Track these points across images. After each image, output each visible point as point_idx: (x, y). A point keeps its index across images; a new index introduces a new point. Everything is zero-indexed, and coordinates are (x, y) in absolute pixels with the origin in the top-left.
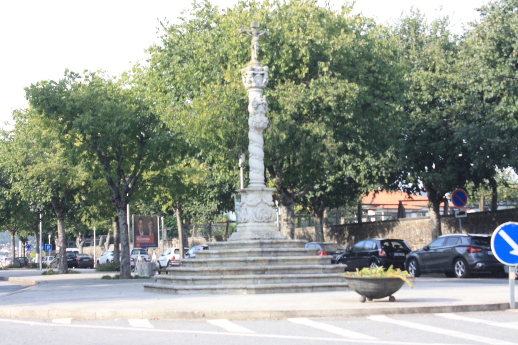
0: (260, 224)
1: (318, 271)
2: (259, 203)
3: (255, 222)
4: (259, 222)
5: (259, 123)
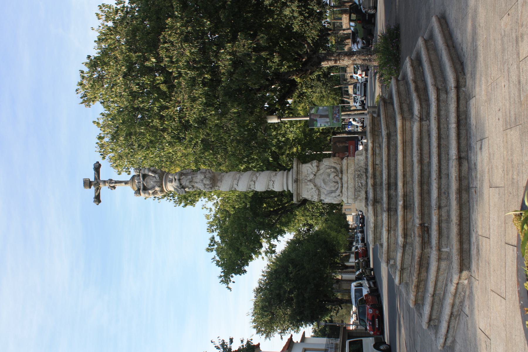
0: (345, 186)
1: (425, 128)
2: (315, 186)
3: (341, 192)
4: (342, 187)
5: (205, 185)
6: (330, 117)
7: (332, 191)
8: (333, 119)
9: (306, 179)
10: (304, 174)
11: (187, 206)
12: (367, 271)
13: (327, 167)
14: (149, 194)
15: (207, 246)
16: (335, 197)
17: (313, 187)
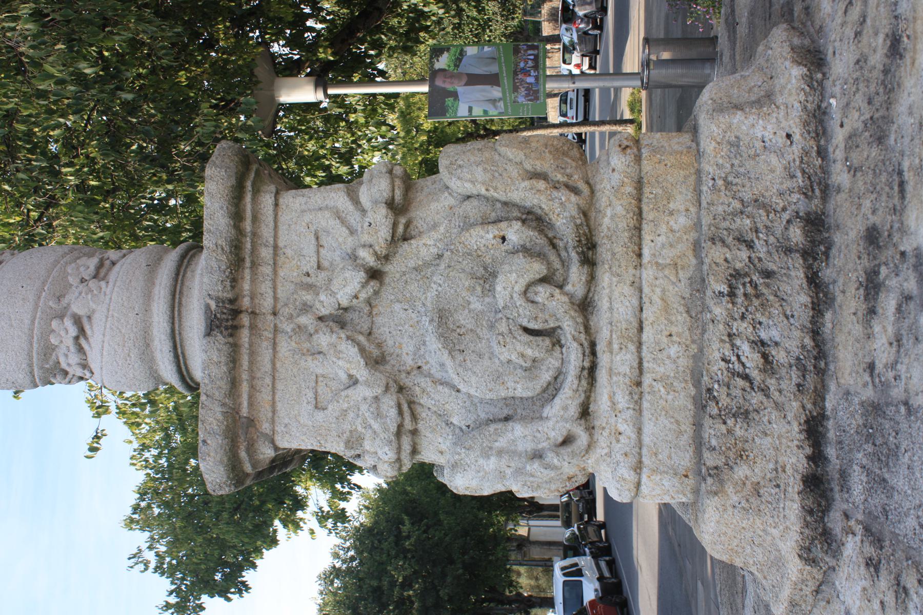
0: (616, 362)
2: (376, 360)
3: (585, 413)
4: (591, 372)
6: (506, 81)
7: (509, 401)
8: (515, 89)
9: (306, 308)
10: (289, 272)
12: (590, 529)
13: (472, 209)
15: (129, 511)
16: (537, 455)
17: (361, 372)
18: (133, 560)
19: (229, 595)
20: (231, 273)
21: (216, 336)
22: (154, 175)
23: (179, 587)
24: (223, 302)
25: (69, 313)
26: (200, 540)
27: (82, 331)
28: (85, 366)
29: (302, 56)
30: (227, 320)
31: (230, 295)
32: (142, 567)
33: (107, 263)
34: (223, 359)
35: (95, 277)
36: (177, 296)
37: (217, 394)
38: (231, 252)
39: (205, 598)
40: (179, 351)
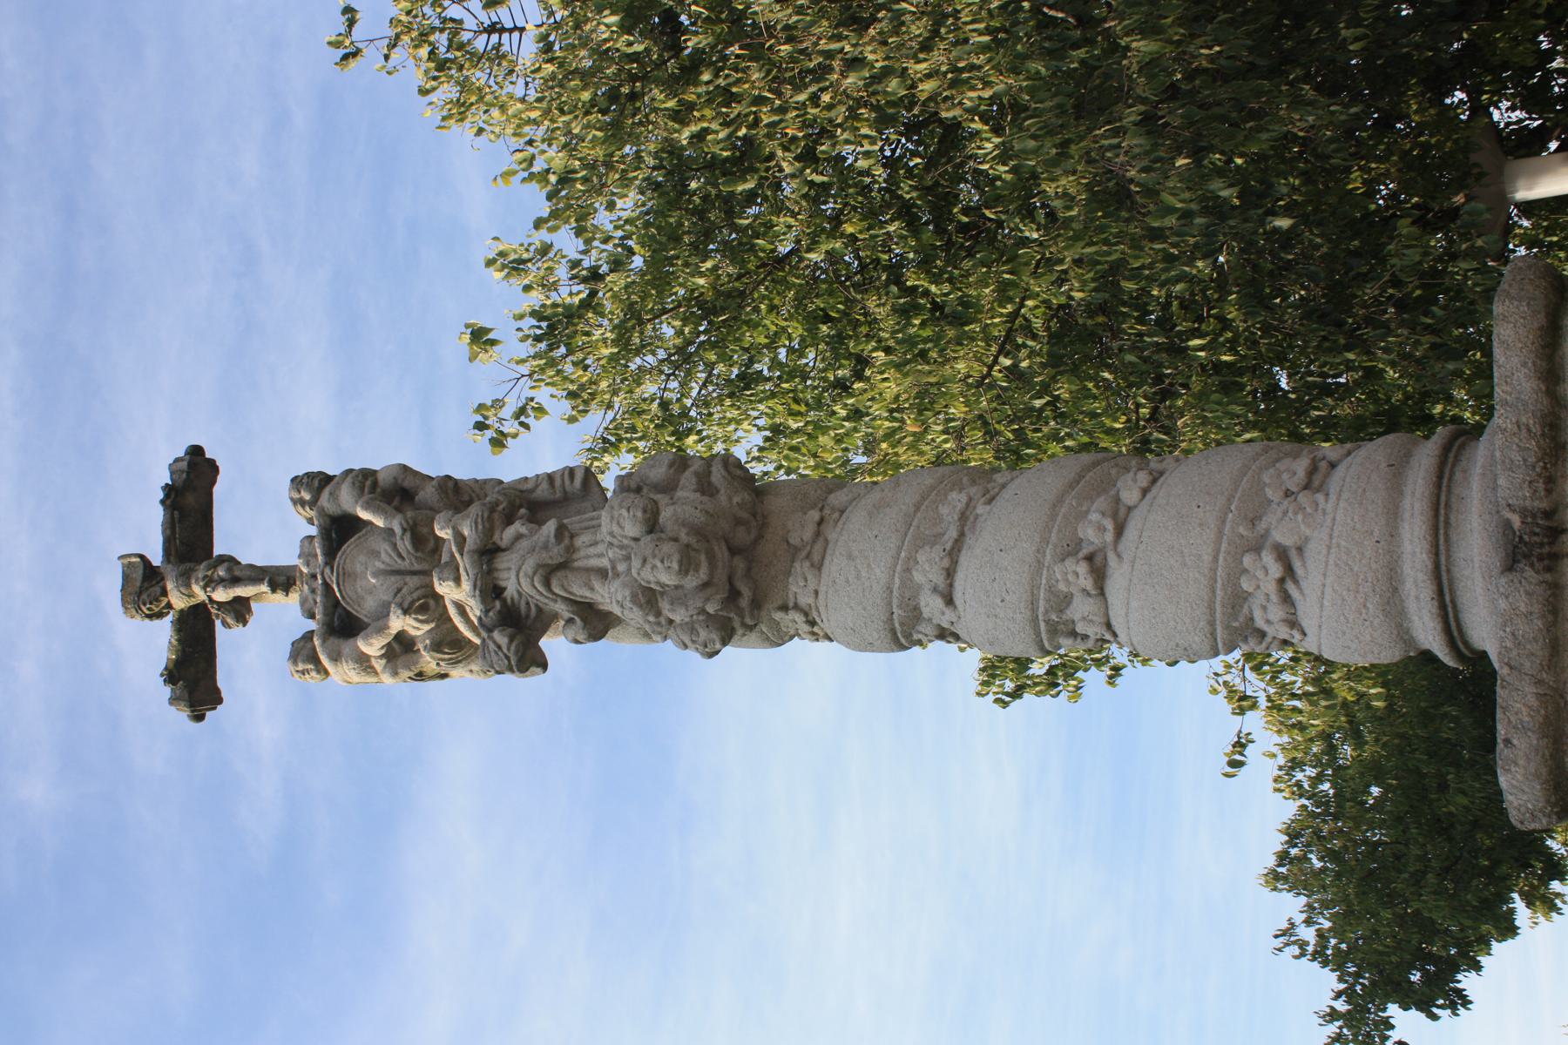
11: (1028, 697)
14: (363, 662)
15: (1271, 861)
18: (1281, 939)
19: (1435, 1010)
20: (1545, 468)
21: (1523, 571)
22: (1325, 338)
23: (1351, 988)
24: (1534, 516)
25: (1268, 544)
26: (1387, 914)
27: (1289, 570)
28: (1293, 624)
29: (1545, 120)
30: (1542, 545)
31: (1544, 505)
32: (1297, 951)
33: (1323, 464)
34: (1536, 608)
35: (1306, 487)
36: (1442, 512)
37: (1528, 664)
38: (1543, 435)
39: (1393, 1010)
40: (1447, 598)
